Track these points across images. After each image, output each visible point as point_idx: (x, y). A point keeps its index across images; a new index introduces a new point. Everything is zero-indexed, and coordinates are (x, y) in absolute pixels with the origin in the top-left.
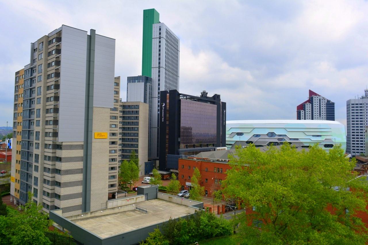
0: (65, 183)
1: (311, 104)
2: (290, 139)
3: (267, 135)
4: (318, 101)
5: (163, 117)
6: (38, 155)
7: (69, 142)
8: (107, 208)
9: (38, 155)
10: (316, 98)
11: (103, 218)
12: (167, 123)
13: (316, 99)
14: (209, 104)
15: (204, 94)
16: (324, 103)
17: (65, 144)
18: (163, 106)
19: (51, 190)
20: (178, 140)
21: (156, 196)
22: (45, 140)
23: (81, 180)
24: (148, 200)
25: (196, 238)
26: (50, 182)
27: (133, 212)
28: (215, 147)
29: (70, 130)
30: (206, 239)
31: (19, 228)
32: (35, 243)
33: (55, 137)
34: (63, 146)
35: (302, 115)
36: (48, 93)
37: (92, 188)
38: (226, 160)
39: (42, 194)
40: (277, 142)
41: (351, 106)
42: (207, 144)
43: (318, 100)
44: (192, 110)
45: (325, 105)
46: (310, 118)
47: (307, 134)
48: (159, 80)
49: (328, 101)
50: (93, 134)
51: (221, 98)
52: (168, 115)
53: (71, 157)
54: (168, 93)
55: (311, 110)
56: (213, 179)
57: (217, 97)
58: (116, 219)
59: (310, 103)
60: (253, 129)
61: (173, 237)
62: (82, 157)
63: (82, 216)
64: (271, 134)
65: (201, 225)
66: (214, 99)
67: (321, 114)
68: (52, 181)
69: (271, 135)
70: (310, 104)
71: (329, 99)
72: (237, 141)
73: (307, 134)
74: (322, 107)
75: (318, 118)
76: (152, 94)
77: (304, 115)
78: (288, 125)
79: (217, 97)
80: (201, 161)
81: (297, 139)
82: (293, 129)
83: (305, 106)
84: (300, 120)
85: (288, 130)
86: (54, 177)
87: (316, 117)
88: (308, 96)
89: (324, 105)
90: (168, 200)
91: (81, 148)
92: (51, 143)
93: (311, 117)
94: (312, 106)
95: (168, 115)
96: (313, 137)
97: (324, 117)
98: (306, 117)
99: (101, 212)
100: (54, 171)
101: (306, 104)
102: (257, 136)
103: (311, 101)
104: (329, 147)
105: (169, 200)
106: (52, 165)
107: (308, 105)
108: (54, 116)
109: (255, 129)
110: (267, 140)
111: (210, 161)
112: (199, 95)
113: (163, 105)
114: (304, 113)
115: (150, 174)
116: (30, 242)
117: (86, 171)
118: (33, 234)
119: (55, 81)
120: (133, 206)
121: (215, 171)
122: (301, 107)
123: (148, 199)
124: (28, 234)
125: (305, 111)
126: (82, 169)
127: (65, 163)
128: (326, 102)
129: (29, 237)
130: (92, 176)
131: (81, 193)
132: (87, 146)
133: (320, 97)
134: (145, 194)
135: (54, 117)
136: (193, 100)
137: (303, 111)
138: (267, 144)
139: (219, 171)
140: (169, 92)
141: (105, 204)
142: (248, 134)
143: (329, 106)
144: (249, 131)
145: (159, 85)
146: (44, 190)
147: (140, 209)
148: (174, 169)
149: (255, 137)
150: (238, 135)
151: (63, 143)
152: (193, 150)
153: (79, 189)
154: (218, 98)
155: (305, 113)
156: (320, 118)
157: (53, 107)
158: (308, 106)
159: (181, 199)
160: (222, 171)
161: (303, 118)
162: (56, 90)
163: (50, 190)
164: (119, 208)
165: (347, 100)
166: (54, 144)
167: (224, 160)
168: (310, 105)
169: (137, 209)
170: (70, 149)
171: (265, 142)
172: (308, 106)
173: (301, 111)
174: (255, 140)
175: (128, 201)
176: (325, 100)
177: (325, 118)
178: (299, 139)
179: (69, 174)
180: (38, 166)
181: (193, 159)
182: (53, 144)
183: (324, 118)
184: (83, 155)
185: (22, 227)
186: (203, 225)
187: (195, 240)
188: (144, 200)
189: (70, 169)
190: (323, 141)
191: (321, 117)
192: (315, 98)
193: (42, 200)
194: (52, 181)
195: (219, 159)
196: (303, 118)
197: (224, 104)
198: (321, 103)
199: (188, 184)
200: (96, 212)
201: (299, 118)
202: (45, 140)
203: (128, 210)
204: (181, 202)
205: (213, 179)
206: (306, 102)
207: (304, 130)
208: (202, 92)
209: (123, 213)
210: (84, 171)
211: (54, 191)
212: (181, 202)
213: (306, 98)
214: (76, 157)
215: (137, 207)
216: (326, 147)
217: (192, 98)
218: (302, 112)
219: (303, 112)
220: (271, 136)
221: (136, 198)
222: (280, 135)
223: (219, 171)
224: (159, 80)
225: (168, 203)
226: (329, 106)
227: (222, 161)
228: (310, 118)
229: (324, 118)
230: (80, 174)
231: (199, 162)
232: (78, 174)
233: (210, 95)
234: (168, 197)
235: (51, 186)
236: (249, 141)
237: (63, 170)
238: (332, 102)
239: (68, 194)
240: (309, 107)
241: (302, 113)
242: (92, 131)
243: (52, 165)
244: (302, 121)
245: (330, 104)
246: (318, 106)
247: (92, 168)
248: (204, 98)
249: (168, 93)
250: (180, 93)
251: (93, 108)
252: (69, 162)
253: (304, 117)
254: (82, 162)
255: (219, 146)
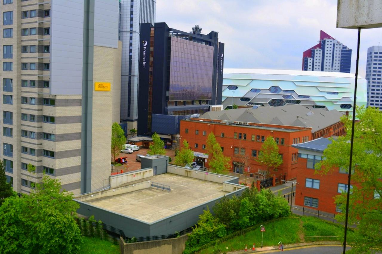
0: (61, 152)
1: (322, 50)
2: (299, 96)
3: (270, 90)
4: (332, 46)
5: (144, 61)
6: (11, 113)
7: (61, 95)
8: (110, 185)
9: (11, 113)
10: (330, 42)
11: (118, 198)
12: (151, 69)
13: (329, 43)
14: (204, 44)
15: (197, 30)
16: (338, 49)
17: (60, 98)
18: (144, 45)
19: (38, 161)
20: (166, 94)
21: (166, 169)
22: (22, 92)
23: (79, 148)
24: (156, 175)
25: (253, 221)
26: (36, 151)
27: (150, 190)
28: (210, 105)
29: (64, 80)
30: (264, 221)
31: (44, 212)
32: (68, 231)
33: (40, 87)
34: (57, 100)
35: (309, 64)
36: (25, 22)
37: (93, 160)
38: (246, 123)
39: (20, 167)
40: (282, 100)
41: (374, 55)
42: (184, 101)
43: (331, 45)
44: (184, 52)
45: (340, 53)
46: (319, 69)
47: (321, 90)
48: (132, 7)
49: (344, 47)
50: (94, 84)
51: (219, 36)
52: (151, 59)
53: (66, 117)
54: (153, 27)
55: (321, 59)
56: (231, 147)
57: (213, 35)
58: (137, 200)
59: (320, 48)
60: (249, 81)
61: (230, 219)
62: (80, 116)
63: (91, 197)
64: (275, 89)
65: (260, 205)
66: (211, 38)
67: (334, 64)
68: (38, 150)
69: (274, 90)
70: (320, 50)
71: (345, 45)
72: (228, 97)
73: (321, 90)
74: (336, 54)
75: (329, 69)
76: (121, 26)
77: (311, 64)
78: (291, 76)
79: (213, 35)
80: (214, 123)
81: (308, 97)
82: (316, 83)
83: (314, 52)
84: (306, 71)
85: (297, 84)
86: (41, 144)
87: (328, 67)
88: (319, 40)
89: (338, 52)
90: (184, 175)
91: (79, 104)
92: (36, 96)
93: (320, 67)
94: (323, 53)
95: (151, 59)
96: (328, 94)
97: (337, 68)
98: (315, 67)
99: (113, 191)
100: (41, 135)
101: (316, 50)
102: (256, 90)
103: (322, 45)
104: (346, 108)
105: (186, 175)
106: (38, 127)
107: (318, 51)
108: (39, 57)
109: (254, 82)
110: (268, 97)
111: (225, 124)
112: (188, 30)
113: (144, 44)
114: (312, 61)
115: (129, 141)
116: (62, 230)
117: (85, 136)
118: (65, 220)
119: (39, 5)
120: (148, 183)
121: (236, 137)
122: (309, 54)
123: (157, 174)
124: (58, 220)
125: (313, 58)
126: (80, 133)
127: (60, 125)
128: (342, 48)
129: (60, 224)
130: (93, 142)
131: (80, 166)
132: (86, 102)
133: (334, 40)
134: (154, 167)
135: (39, 59)
136: (185, 39)
137: (311, 58)
138: (268, 102)
139: (241, 137)
140: (154, 26)
141: (107, 181)
142: (244, 87)
143: (345, 54)
144: (245, 83)
145: (132, 13)
146: (23, 162)
147: (158, 187)
148: (167, 135)
149: (254, 92)
150: (229, 89)
151: (57, 96)
152: (175, 109)
153: (77, 161)
154: (215, 36)
155: (313, 61)
156: (332, 69)
157: (37, 44)
158: (318, 52)
159: (205, 173)
160: (245, 138)
161: (310, 69)
162: (40, 18)
163: (37, 163)
164: (134, 185)
165: (368, 47)
166: (40, 97)
167: (244, 123)
168: (320, 51)
169: (153, 187)
170: (66, 105)
171: (266, 99)
172: (318, 53)
173: (309, 58)
174: (252, 96)
175: (134, 176)
176: (340, 45)
177: (338, 69)
178: (311, 97)
179: (65, 141)
180: (11, 129)
181: (199, 121)
182: (38, 98)
183: (337, 69)
184: (81, 113)
185: (48, 210)
186: (263, 205)
187: (253, 223)
188: (152, 175)
189: (67, 133)
190: (340, 99)
191: (334, 67)
192: (328, 41)
193: (21, 176)
194: (38, 150)
195: (237, 122)
196: (310, 69)
197: (222, 45)
198: (335, 49)
199: (194, 154)
200: (107, 191)
201: (305, 68)
202: (22, 92)
203: (142, 188)
204: (205, 177)
205: (231, 147)
206: (315, 47)
207: (305, 84)
208: (194, 27)
209: (138, 192)
210: (83, 136)
211: (42, 163)
212: (205, 177)
213: (316, 41)
214: (73, 117)
215: (153, 184)
216: (343, 108)
217: (184, 35)
218: (310, 60)
219: (310, 60)
220: (275, 92)
221: (144, 173)
222: (287, 91)
223: (241, 137)
224: (132, 7)
225: (186, 179)
226: (345, 54)
227: (240, 124)
228: (319, 69)
229: (337, 69)
230: (78, 140)
231: (211, 125)
232: (76, 141)
233: (205, 32)
234: (184, 171)
235: (38, 156)
236: (244, 98)
237: (57, 135)
238: (349, 48)
239: (64, 167)
240: (320, 54)
241: (309, 61)
242: (92, 81)
243: (38, 127)
244: (309, 73)
245: (347, 50)
246: (331, 52)
247: (93, 131)
248: (196, 36)
249: (153, 27)
250: (170, 27)
251: (93, 47)
252: (65, 123)
253: (311, 67)
254: (80, 123)
255: (214, 104)
